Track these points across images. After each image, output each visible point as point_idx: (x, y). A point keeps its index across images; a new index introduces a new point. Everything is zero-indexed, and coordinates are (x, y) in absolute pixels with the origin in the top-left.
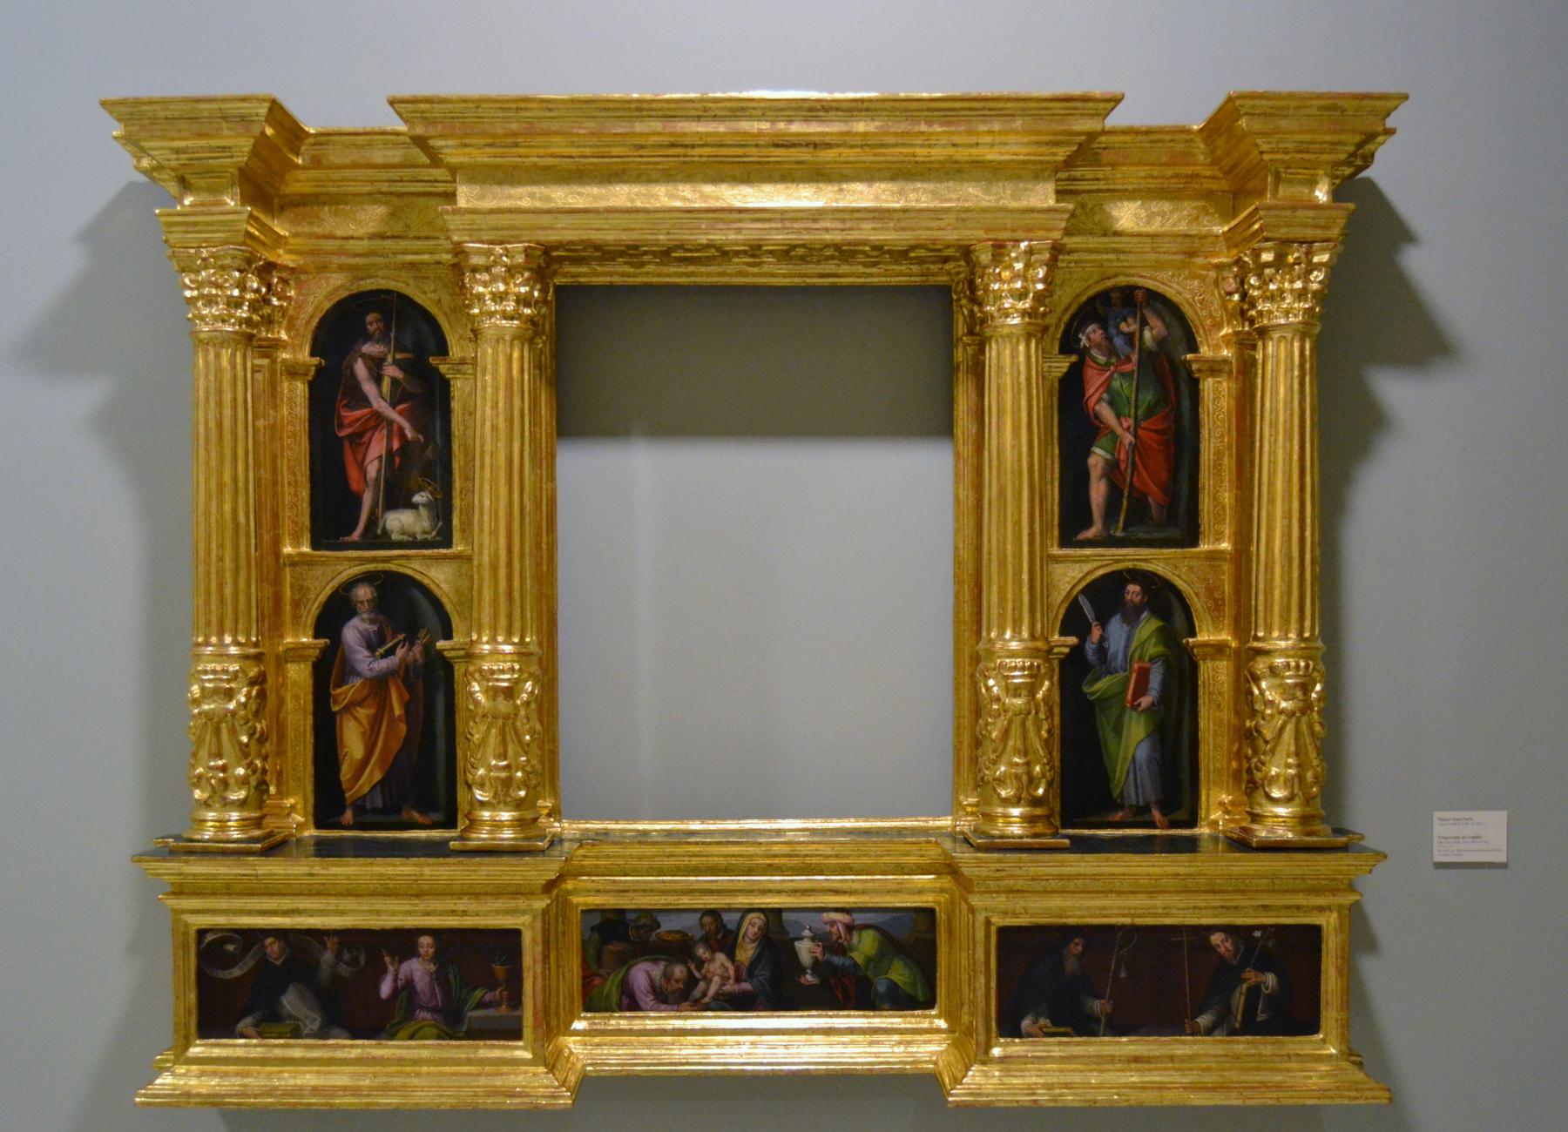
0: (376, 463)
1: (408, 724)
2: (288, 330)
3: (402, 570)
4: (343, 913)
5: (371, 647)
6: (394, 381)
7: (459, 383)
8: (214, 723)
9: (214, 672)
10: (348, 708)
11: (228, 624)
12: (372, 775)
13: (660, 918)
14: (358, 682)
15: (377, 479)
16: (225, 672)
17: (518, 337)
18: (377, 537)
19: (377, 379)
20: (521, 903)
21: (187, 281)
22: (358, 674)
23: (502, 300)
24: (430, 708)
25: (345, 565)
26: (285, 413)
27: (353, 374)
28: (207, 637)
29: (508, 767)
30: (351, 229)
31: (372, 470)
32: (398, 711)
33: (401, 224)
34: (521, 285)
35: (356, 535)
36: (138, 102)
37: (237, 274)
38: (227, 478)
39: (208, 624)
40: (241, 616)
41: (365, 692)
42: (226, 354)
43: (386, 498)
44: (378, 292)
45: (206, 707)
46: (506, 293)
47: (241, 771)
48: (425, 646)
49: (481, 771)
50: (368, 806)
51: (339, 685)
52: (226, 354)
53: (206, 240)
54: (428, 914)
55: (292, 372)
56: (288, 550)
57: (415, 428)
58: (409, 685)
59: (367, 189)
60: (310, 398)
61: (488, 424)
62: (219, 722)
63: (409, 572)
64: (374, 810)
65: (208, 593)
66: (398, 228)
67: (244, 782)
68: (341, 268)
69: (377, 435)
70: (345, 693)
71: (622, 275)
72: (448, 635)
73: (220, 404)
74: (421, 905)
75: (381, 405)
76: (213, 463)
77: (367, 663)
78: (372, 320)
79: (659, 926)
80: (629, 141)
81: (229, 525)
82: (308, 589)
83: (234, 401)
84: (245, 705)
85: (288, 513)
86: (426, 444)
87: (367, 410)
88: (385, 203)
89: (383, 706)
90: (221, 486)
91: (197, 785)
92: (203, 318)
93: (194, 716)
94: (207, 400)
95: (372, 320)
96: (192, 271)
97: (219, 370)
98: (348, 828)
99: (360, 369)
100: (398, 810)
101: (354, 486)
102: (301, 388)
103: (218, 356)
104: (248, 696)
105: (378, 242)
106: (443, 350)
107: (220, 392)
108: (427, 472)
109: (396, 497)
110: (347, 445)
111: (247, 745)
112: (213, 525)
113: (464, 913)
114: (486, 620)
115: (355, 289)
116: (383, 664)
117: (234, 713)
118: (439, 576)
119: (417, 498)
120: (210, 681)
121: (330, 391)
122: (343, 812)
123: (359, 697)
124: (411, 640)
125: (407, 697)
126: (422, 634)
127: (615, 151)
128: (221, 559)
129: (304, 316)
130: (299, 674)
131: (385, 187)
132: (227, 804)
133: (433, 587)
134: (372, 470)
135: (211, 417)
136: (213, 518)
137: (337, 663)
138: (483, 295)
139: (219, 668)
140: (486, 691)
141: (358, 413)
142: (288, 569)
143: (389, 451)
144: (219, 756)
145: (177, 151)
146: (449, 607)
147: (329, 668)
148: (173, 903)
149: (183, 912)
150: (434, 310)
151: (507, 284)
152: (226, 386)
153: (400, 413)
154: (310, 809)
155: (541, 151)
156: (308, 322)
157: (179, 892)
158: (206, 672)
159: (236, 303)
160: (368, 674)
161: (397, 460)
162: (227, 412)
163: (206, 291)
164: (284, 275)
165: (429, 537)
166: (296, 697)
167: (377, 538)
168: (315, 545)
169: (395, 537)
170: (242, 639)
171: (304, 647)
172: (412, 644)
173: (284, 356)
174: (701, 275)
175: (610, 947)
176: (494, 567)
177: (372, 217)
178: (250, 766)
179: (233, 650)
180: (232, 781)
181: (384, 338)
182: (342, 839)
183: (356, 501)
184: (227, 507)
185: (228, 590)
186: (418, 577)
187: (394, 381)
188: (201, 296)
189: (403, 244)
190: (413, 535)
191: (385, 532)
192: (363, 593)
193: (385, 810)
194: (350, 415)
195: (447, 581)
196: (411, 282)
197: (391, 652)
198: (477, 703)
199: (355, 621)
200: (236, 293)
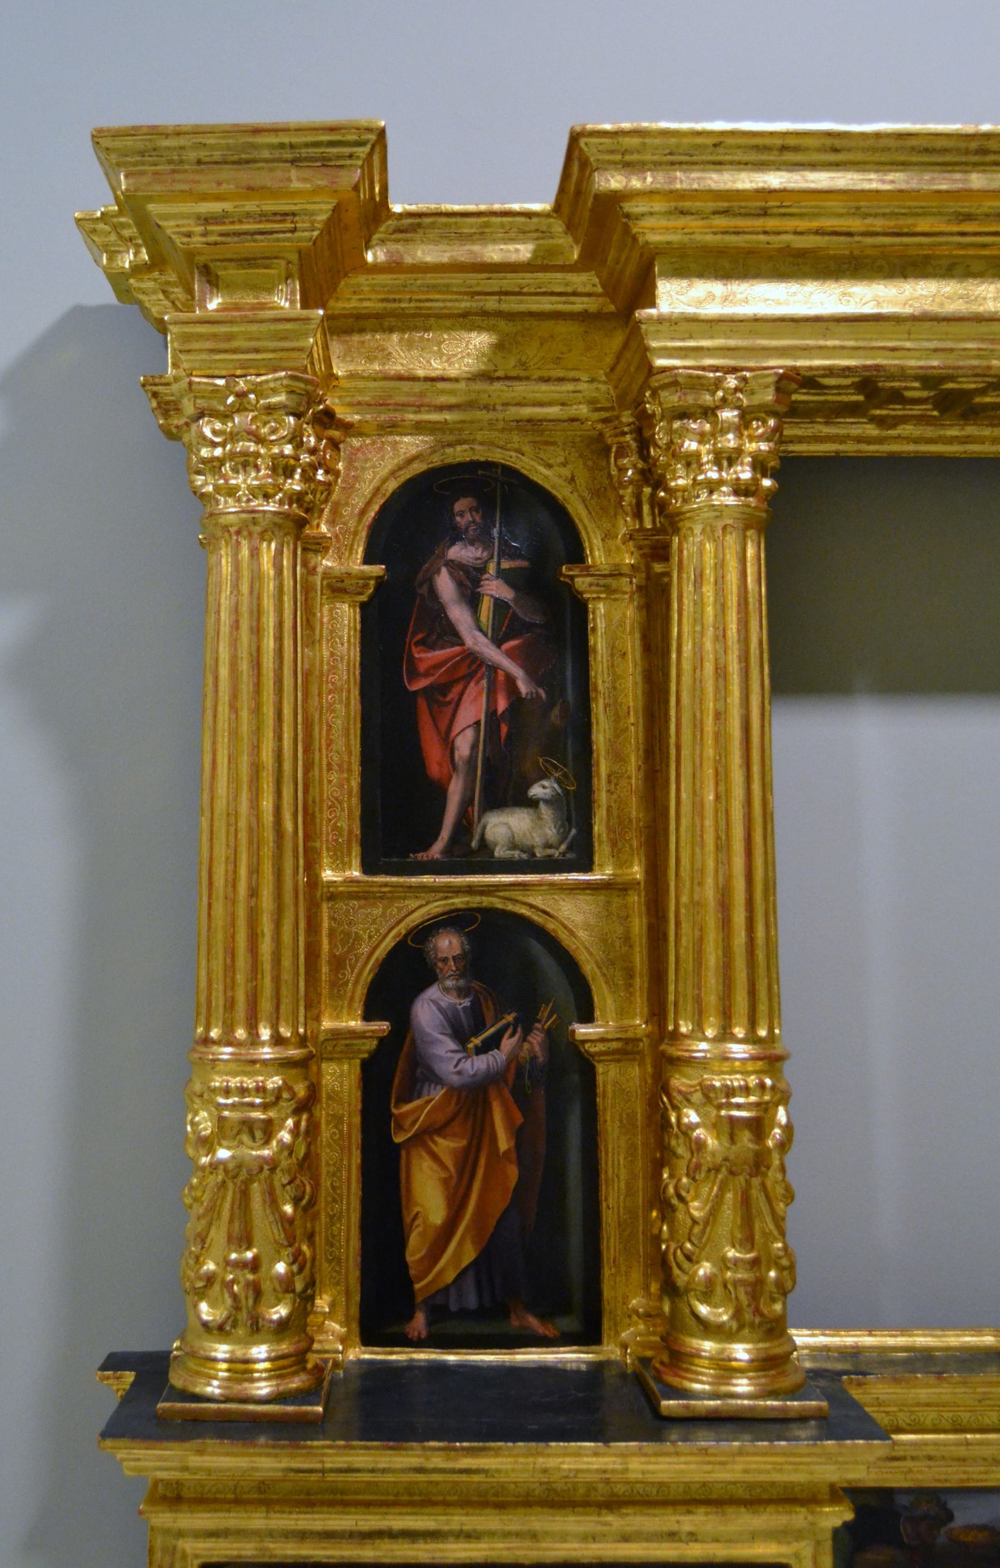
0: (470, 733)
1: (520, 1163)
2: (332, 523)
3: (510, 907)
4: (469, 1536)
5: (460, 1034)
6: (499, 604)
7: (601, 608)
8: (239, 1177)
9: (243, 1091)
10: (422, 1138)
11: (266, 1005)
12: (462, 1252)
13: (953, 1504)
14: (438, 1094)
15: (471, 761)
16: (260, 1090)
17: (748, 523)
18: (472, 852)
19: (473, 601)
20: (799, 1518)
21: (207, 432)
22: (437, 1080)
23: (731, 462)
24: (556, 1138)
25: (425, 895)
26: (326, 654)
27: (433, 593)
28: (229, 1028)
29: (755, 1263)
30: (437, 367)
31: (463, 746)
32: (504, 1143)
33: (512, 362)
34: (760, 438)
35: (436, 850)
36: (156, 132)
37: (291, 419)
38: (267, 756)
39: (230, 1005)
40: (284, 992)
41: (452, 1108)
42: (268, 551)
43: (486, 788)
44: (474, 466)
45: (223, 1154)
46: (739, 451)
47: (281, 1268)
48: (548, 1033)
49: (704, 1269)
50: (453, 1307)
51: (406, 1097)
52: (268, 551)
53: (244, 365)
54: (626, 1538)
55: (338, 587)
56: (328, 875)
57: (532, 674)
58: (521, 1098)
59: (465, 305)
60: (363, 631)
61: (709, 667)
62: (247, 1183)
63: (524, 911)
64: (464, 1314)
65: (231, 952)
66: (508, 365)
67: (286, 1285)
68: (419, 428)
69: (472, 689)
70: (415, 1112)
71: (859, 440)
72: (587, 1017)
73: (257, 631)
74: (615, 1522)
75: (477, 641)
76: (245, 729)
77: (453, 1062)
78: (464, 511)
79: (950, 1517)
80: (953, 206)
81: (269, 835)
82: (358, 938)
83: (273, 621)
84: (289, 1149)
85: (326, 814)
86: (550, 706)
87: (457, 649)
88: (488, 329)
89: (480, 1134)
90: (256, 768)
91: (201, 1294)
92: (232, 492)
93: (203, 1168)
94: (236, 626)
95: (464, 511)
96: (214, 414)
97: (257, 577)
98: (419, 1344)
99: (445, 584)
100: (500, 1311)
101: (434, 770)
102: (346, 616)
103: (255, 553)
104: (295, 1132)
105: (479, 386)
106: (576, 554)
107: (257, 613)
108: (552, 748)
109: (503, 790)
110: (422, 705)
111: (291, 1221)
112: (243, 836)
113: (693, 1537)
114: (711, 999)
115: (437, 460)
116: (480, 1064)
117: (273, 1164)
118: (569, 911)
119: (536, 791)
120: (233, 1106)
121: (395, 620)
122: (410, 1317)
123: (441, 1118)
124: (526, 1024)
125: (519, 1119)
126: (544, 1012)
127: (924, 225)
128: (254, 893)
129: (358, 502)
130: (341, 1078)
131: (491, 304)
132: (256, 1328)
133: (563, 936)
134: (463, 746)
135: (244, 652)
136: (243, 824)
137: (402, 1064)
138: (698, 455)
139: (249, 1083)
140: (715, 1126)
141: (440, 654)
142: (325, 906)
143: (491, 714)
144: (246, 1240)
145: (207, 220)
146: (589, 968)
147: (390, 1070)
148: (164, 1519)
149: (180, 1534)
150: (562, 492)
151: (740, 436)
152: (268, 604)
153: (510, 654)
154: (355, 1311)
155: (803, 224)
156: (363, 512)
157: (173, 1496)
158: (227, 1092)
159: (283, 468)
160: (455, 1080)
161: (504, 729)
162: (269, 643)
163: (239, 446)
164: (336, 434)
165: (556, 853)
166: (336, 1120)
167: (471, 855)
168: (368, 868)
169: (500, 853)
170: (286, 1032)
171: (353, 1034)
172: (527, 1031)
173: (327, 563)
174: (981, 440)
175: (869, 1556)
176: (725, 906)
177: (465, 352)
178: (296, 1258)
179: (267, 1052)
180: (266, 1287)
181: (483, 538)
182: (411, 1367)
183: (440, 792)
184: (267, 804)
185: (266, 947)
186: (537, 918)
187: (499, 604)
188: (232, 456)
189: (520, 389)
190: (530, 851)
191: (485, 846)
192: (448, 944)
193: (480, 1314)
194: (427, 657)
195: (587, 926)
196: (527, 448)
197: (492, 1044)
198: (700, 1145)
199: (433, 992)
200: (288, 449)
